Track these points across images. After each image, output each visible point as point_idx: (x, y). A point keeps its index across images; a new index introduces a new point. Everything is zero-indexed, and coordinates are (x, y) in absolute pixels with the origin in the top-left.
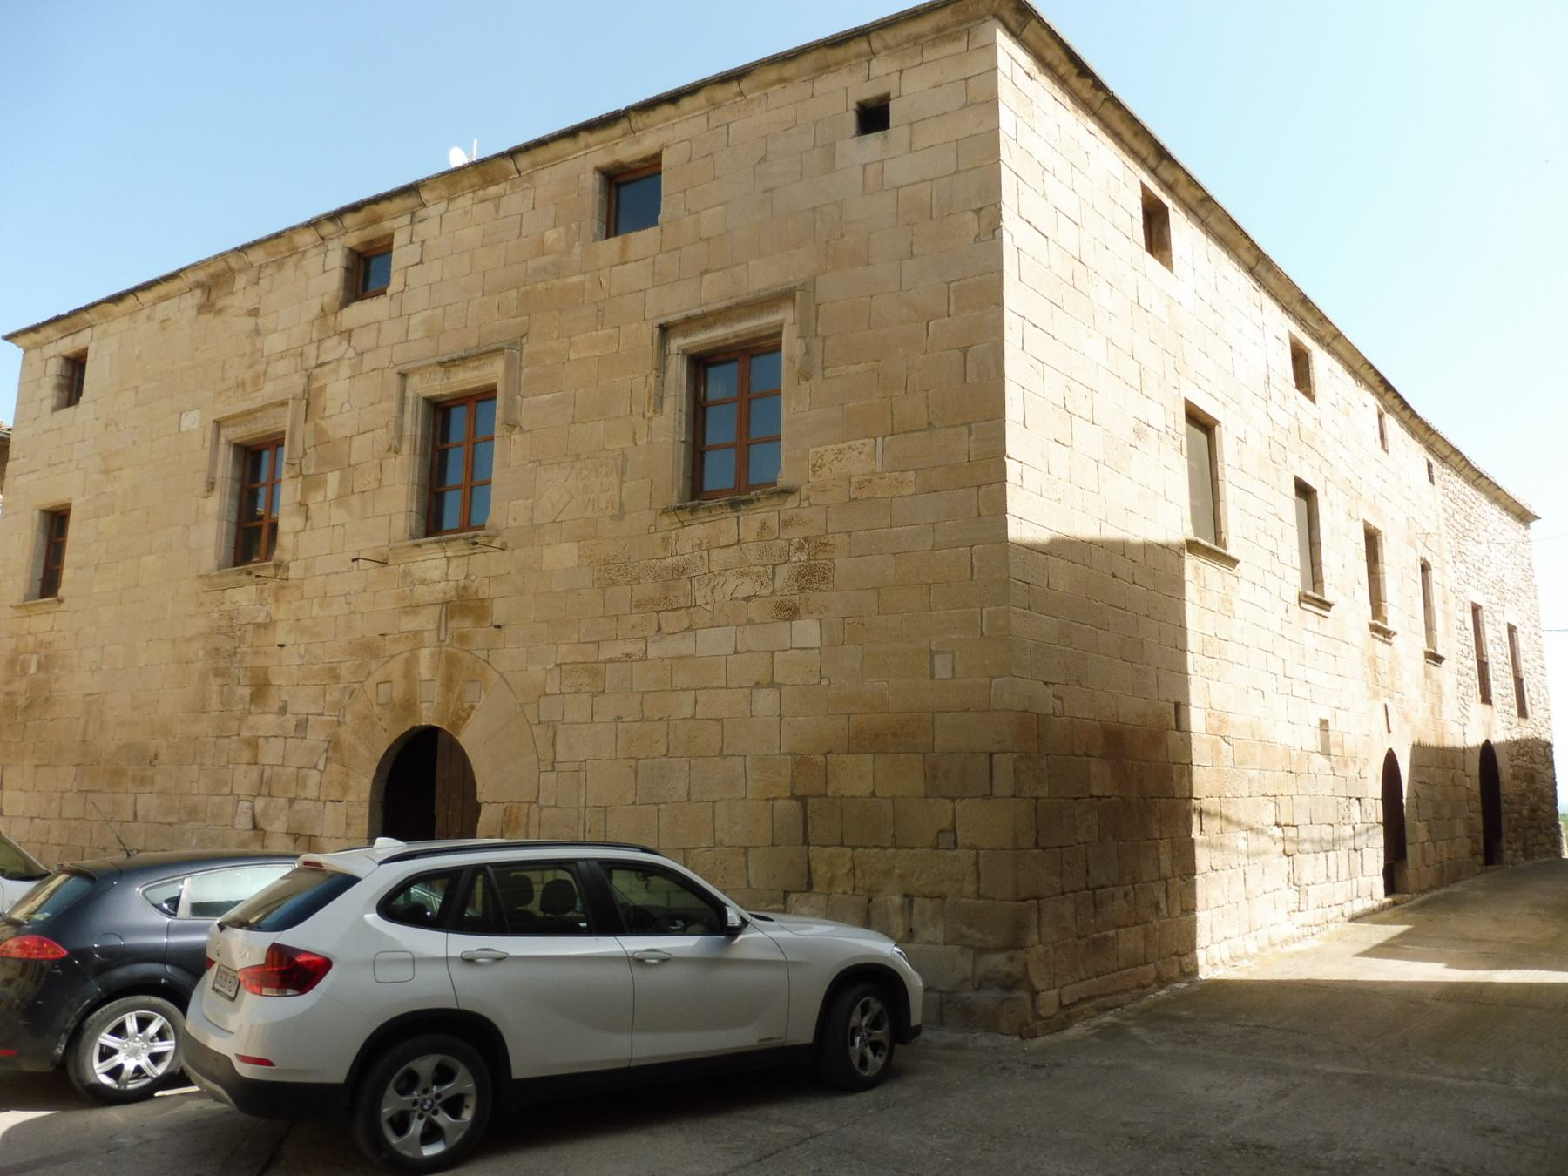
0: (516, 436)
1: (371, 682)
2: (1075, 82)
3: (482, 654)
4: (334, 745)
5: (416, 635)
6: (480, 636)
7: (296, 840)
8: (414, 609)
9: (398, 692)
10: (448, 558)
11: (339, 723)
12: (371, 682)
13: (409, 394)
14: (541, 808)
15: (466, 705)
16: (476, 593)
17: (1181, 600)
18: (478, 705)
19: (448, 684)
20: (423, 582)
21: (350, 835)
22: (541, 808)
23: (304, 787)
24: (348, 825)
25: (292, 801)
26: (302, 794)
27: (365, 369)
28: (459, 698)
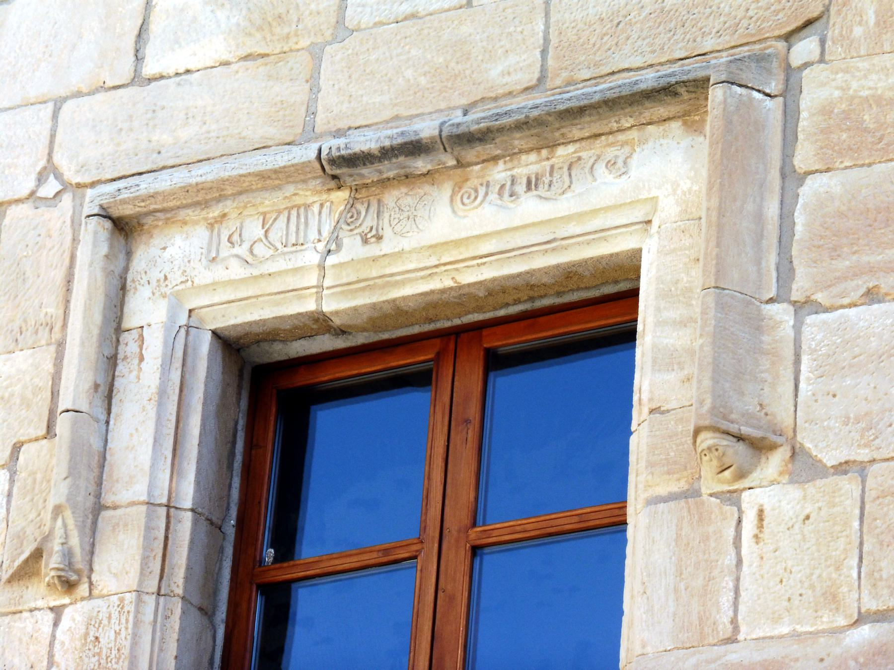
0: (770, 492)
2: (328, 557)
13: (148, 311)
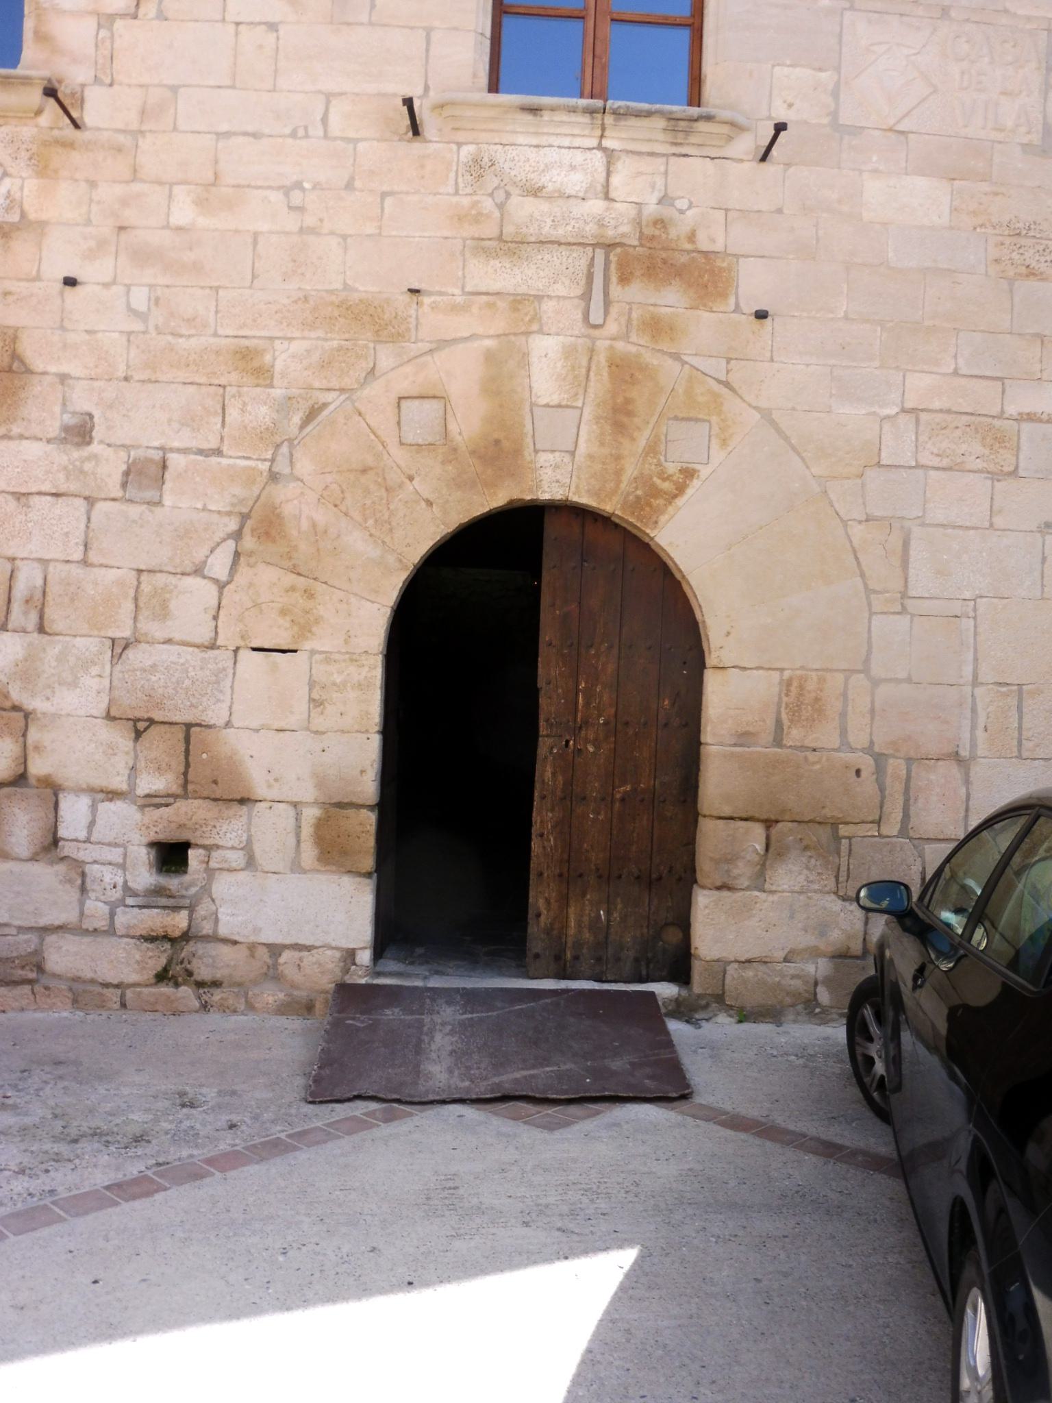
1: (377, 395)
3: (715, 367)
4: (259, 527)
5: (523, 307)
6: (704, 330)
7: (138, 734)
8: (510, 246)
9: (467, 425)
10: (610, 155)
11: (274, 477)
12: (377, 395)
14: (876, 683)
15: (672, 468)
16: (692, 237)
17: (528, 879)
18: (704, 471)
19: (619, 417)
20: (535, 192)
21: (319, 722)
22: (876, 683)
23: (163, 613)
24: (315, 703)
25: (120, 648)
26: (156, 630)
27: (286, 443)
28: (652, 449)
